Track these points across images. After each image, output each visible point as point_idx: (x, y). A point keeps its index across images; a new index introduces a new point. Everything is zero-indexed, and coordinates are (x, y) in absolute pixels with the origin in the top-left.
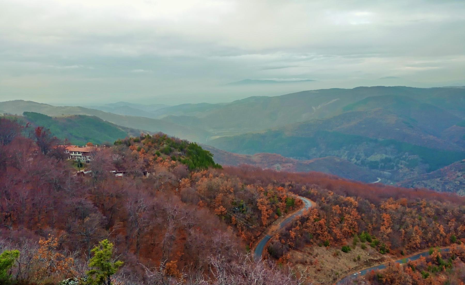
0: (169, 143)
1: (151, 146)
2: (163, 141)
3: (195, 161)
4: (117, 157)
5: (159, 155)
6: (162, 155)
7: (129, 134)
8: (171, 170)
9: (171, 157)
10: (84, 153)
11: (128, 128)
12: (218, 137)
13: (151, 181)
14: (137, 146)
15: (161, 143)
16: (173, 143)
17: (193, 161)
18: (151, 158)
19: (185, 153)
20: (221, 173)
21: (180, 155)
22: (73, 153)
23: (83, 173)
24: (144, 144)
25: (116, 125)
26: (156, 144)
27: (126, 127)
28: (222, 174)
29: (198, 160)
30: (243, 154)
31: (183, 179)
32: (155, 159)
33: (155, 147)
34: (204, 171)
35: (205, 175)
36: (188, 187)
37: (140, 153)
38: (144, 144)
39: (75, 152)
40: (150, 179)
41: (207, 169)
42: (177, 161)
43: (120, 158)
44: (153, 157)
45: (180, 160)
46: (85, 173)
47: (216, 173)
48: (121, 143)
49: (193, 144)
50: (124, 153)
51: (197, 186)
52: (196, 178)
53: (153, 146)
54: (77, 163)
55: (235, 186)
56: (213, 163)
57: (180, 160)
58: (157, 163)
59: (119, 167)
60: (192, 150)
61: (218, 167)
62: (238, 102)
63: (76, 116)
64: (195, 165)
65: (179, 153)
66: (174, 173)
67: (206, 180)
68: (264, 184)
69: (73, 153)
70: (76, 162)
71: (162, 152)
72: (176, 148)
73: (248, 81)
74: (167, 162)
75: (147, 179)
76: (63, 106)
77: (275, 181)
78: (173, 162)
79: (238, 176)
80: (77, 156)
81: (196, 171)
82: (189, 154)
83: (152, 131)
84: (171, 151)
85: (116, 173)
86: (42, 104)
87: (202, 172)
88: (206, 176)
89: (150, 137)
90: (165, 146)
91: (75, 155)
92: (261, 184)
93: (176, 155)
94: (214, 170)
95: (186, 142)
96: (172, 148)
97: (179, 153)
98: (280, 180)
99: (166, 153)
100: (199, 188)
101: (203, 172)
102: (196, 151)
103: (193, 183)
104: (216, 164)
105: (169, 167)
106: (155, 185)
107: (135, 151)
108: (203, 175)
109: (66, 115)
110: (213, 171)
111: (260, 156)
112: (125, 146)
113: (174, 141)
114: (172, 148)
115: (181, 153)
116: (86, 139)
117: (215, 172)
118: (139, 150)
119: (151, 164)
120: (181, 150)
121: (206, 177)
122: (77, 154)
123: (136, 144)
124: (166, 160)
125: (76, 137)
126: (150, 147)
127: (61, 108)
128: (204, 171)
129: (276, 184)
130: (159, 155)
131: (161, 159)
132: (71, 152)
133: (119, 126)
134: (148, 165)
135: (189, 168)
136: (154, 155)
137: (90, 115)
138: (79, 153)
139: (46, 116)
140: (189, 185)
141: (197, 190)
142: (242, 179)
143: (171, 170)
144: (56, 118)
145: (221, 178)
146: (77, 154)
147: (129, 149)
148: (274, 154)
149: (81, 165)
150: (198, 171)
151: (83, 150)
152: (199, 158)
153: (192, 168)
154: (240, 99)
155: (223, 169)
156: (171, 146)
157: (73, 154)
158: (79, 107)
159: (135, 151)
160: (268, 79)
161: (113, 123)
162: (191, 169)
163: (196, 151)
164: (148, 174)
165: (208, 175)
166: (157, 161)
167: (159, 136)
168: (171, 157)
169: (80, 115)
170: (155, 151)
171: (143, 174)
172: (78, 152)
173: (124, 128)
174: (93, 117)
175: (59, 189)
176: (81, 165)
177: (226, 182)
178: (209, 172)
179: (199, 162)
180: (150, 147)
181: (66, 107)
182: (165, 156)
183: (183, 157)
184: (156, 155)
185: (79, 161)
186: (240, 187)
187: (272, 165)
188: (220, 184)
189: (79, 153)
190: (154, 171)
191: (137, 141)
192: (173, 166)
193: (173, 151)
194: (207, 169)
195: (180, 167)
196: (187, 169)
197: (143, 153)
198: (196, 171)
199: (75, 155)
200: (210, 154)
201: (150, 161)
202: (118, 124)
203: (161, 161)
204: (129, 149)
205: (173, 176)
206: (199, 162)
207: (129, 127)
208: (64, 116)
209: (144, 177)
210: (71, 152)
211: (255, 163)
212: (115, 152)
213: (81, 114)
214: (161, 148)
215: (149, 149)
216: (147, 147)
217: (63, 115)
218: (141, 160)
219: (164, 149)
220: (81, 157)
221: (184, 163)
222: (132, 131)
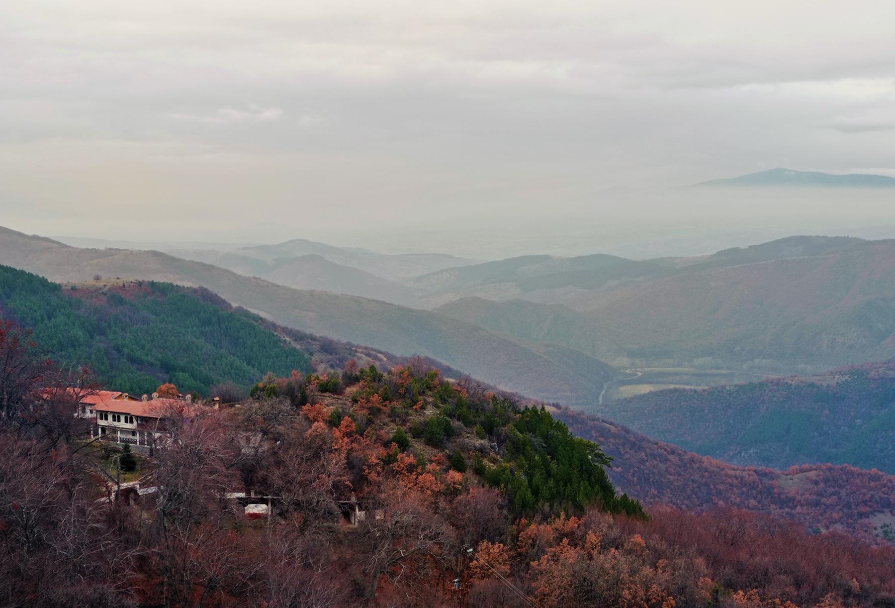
0: (444, 401)
1: (379, 410)
2: (423, 393)
3: (537, 478)
4: (252, 445)
5: (404, 445)
6: (418, 446)
7: (316, 358)
8: (442, 504)
9: (449, 457)
10: (145, 421)
11: (314, 338)
12: (645, 389)
13: (365, 540)
14: (328, 405)
15: (415, 403)
16: (459, 404)
17: (530, 476)
18: (375, 455)
19: (500, 442)
20: (632, 532)
21: (482, 451)
22: (110, 417)
23: (132, 490)
24: (355, 401)
25: (274, 326)
26: (398, 405)
27: (308, 331)
28: (637, 538)
29: (549, 474)
30: (738, 464)
31: (484, 544)
32: (389, 460)
33: (393, 415)
34: (568, 518)
35: (570, 535)
36: (499, 579)
37: (337, 433)
38: (355, 401)
39: (117, 417)
40: (364, 533)
41: (579, 511)
42: (469, 473)
43: (266, 446)
44: (382, 451)
45: (479, 471)
46: (141, 492)
47: (615, 533)
48: (273, 392)
49: (534, 410)
50: (281, 429)
51: (534, 578)
52: (533, 546)
53: (387, 410)
54: (117, 456)
55: (682, 590)
56: (607, 490)
57: (479, 471)
58: (394, 474)
59: (252, 478)
60: (529, 436)
61: (628, 509)
62: (732, 259)
63: (140, 284)
64: (536, 492)
65: (478, 442)
66: (453, 520)
67: (571, 555)
68: (803, 593)
69: (110, 417)
70: (116, 451)
71: (417, 434)
72: (468, 423)
73: (776, 177)
74: (434, 473)
75: (354, 532)
76: (102, 247)
77: (855, 584)
78: (455, 476)
79: (701, 553)
80: (123, 431)
81: (538, 518)
82: (518, 449)
83: (399, 349)
84: (450, 433)
85: (244, 502)
86: (35, 238)
87: (559, 523)
88: (575, 540)
89: (377, 378)
90: (430, 412)
91: (116, 424)
92: (792, 590)
93: (465, 448)
94: (609, 518)
95: (509, 402)
96: (456, 424)
97: (478, 442)
98: (876, 582)
99: (433, 442)
100: (541, 585)
101: (565, 523)
102: (546, 438)
103: (521, 559)
104: (619, 491)
105: (436, 494)
106: (376, 557)
107: (320, 426)
108: (561, 536)
109: (109, 279)
110: (604, 523)
111: (813, 474)
112: (287, 405)
113: (464, 395)
114: (456, 424)
115: (485, 442)
116: (168, 368)
117: (610, 527)
118: (334, 422)
119: (373, 476)
120: (489, 430)
121: (573, 544)
122: (122, 424)
123: (328, 398)
124: (429, 467)
125: (133, 360)
126: (375, 412)
127: (94, 253)
128: (568, 518)
129: (857, 596)
130: (404, 445)
131: (410, 460)
132: (104, 415)
133: (284, 330)
134: (360, 480)
135: (511, 501)
136: (386, 444)
137: (187, 284)
138: (129, 418)
139: (43, 282)
140: (506, 568)
141: (529, 592)
142: (715, 562)
143: (442, 504)
144: (74, 288)
145: (630, 552)
146: (122, 424)
147: (300, 419)
148: (874, 470)
149: (129, 464)
150: (545, 518)
151: (137, 408)
152: (553, 466)
153: (524, 505)
154: (743, 246)
155: (644, 517)
156: (451, 415)
157: (110, 421)
158: (155, 254)
159: (320, 426)
160: (872, 171)
161: (263, 315)
162: (520, 509)
163: (546, 438)
164: (360, 514)
165: (583, 537)
166: (395, 466)
167: (411, 375)
168: (449, 457)
169: (153, 284)
170: (391, 430)
171: (337, 511)
172: (114, 414)
173: (298, 336)
174: (195, 291)
175: (39, 545)
176: (129, 464)
177: (647, 571)
178: (587, 526)
179: (551, 483)
180: (375, 412)
181: (111, 252)
182: (428, 452)
183: (494, 461)
184: (395, 446)
185: (127, 448)
186: (706, 594)
187: (861, 515)
188: (625, 576)
189: (129, 418)
190: (379, 505)
191: (330, 388)
192: (452, 492)
193: (459, 435)
194: (579, 511)
195: (479, 497)
196: (501, 507)
197: (349, 435)
198: (538, 518)
199: (116, 424)
200: (600, 456)
201: (369, 466)
202: (280, 323)
203: (411, 468)
204: (300, 419)
205: (447, 530)
206: (551, 483)
207: (318, 335)
208: (100, 284)
209: (342, 526)
210: (104, 415)
211: (787, 502)
212: (248, 424)
213: (159, 279)
214: (415, 419)
215: (370, 422)
216: (365, 412)
217: (97, 278)
218: (335, 463)
219: (426, 424)
220: (134, 433)
221: (495, 481)
222: (328, 347)
